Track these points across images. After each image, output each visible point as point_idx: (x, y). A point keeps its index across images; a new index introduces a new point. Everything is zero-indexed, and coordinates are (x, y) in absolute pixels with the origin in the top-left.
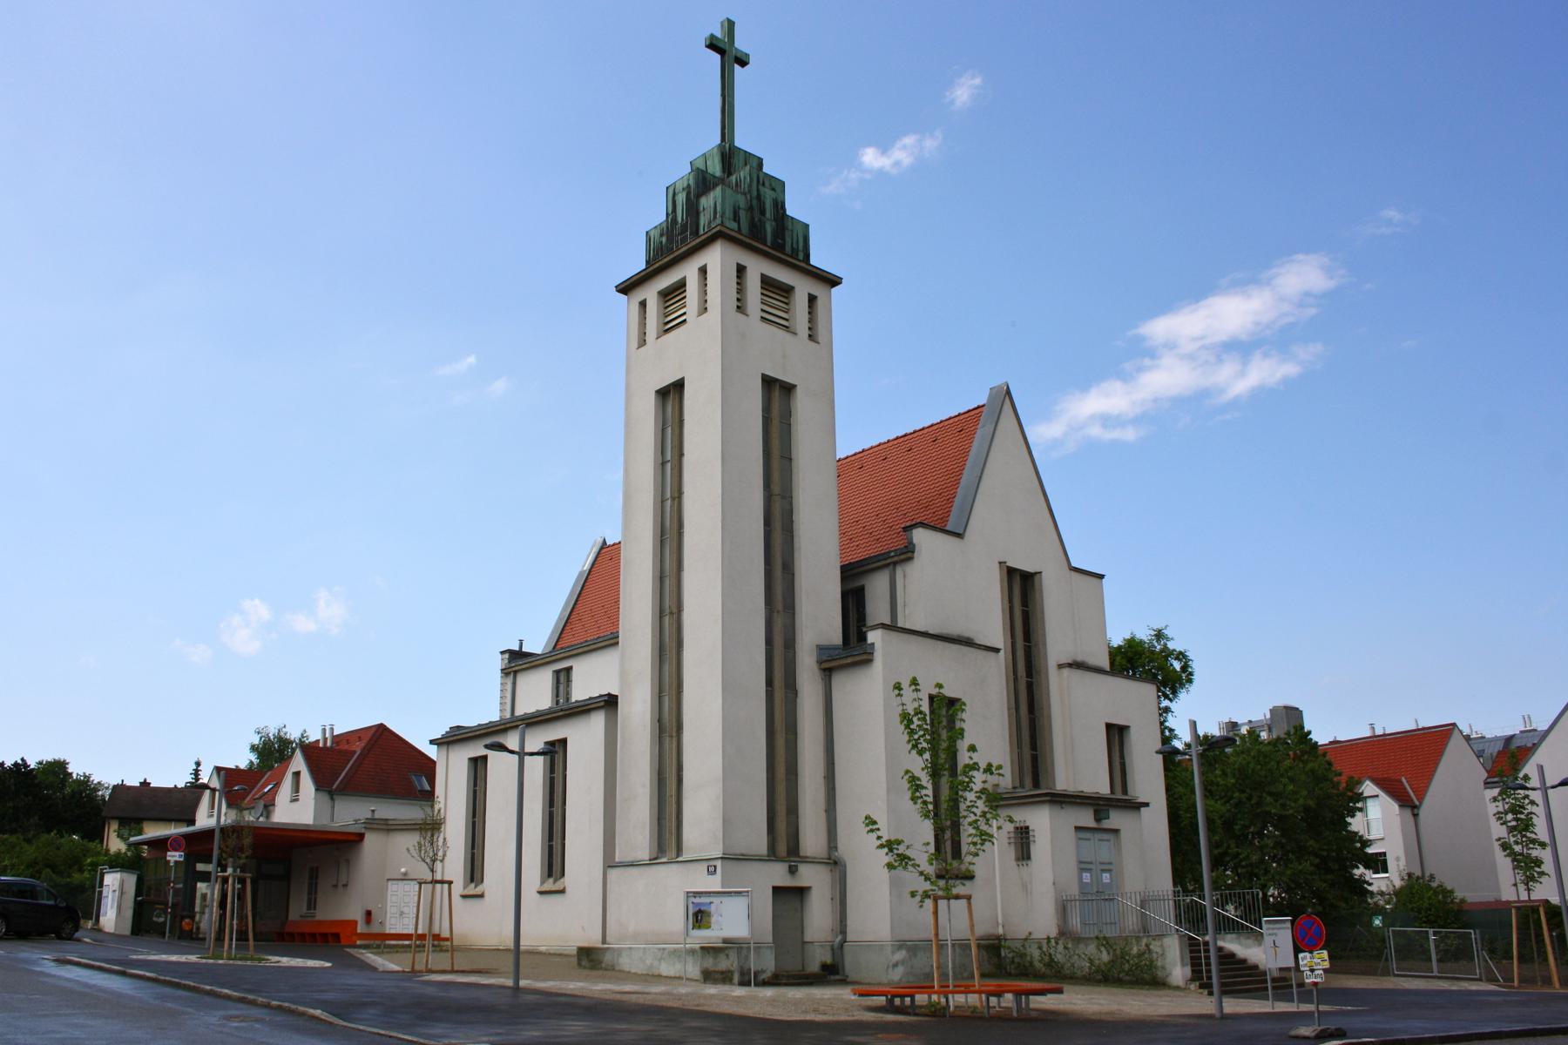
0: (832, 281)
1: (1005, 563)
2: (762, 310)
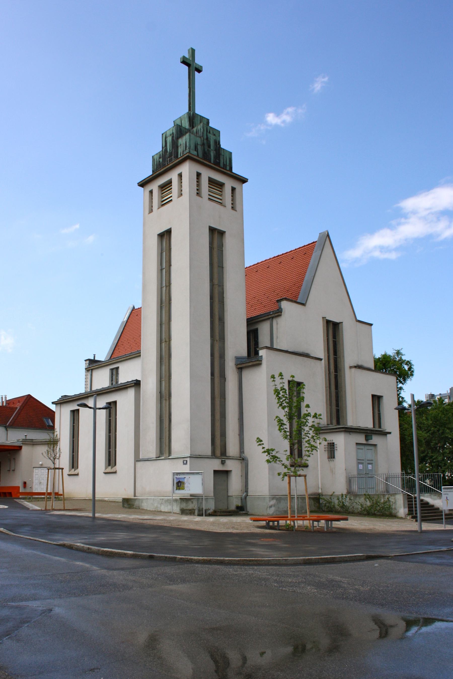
0: (243, 181)
1: (325, 318)
2: (209, 195)
